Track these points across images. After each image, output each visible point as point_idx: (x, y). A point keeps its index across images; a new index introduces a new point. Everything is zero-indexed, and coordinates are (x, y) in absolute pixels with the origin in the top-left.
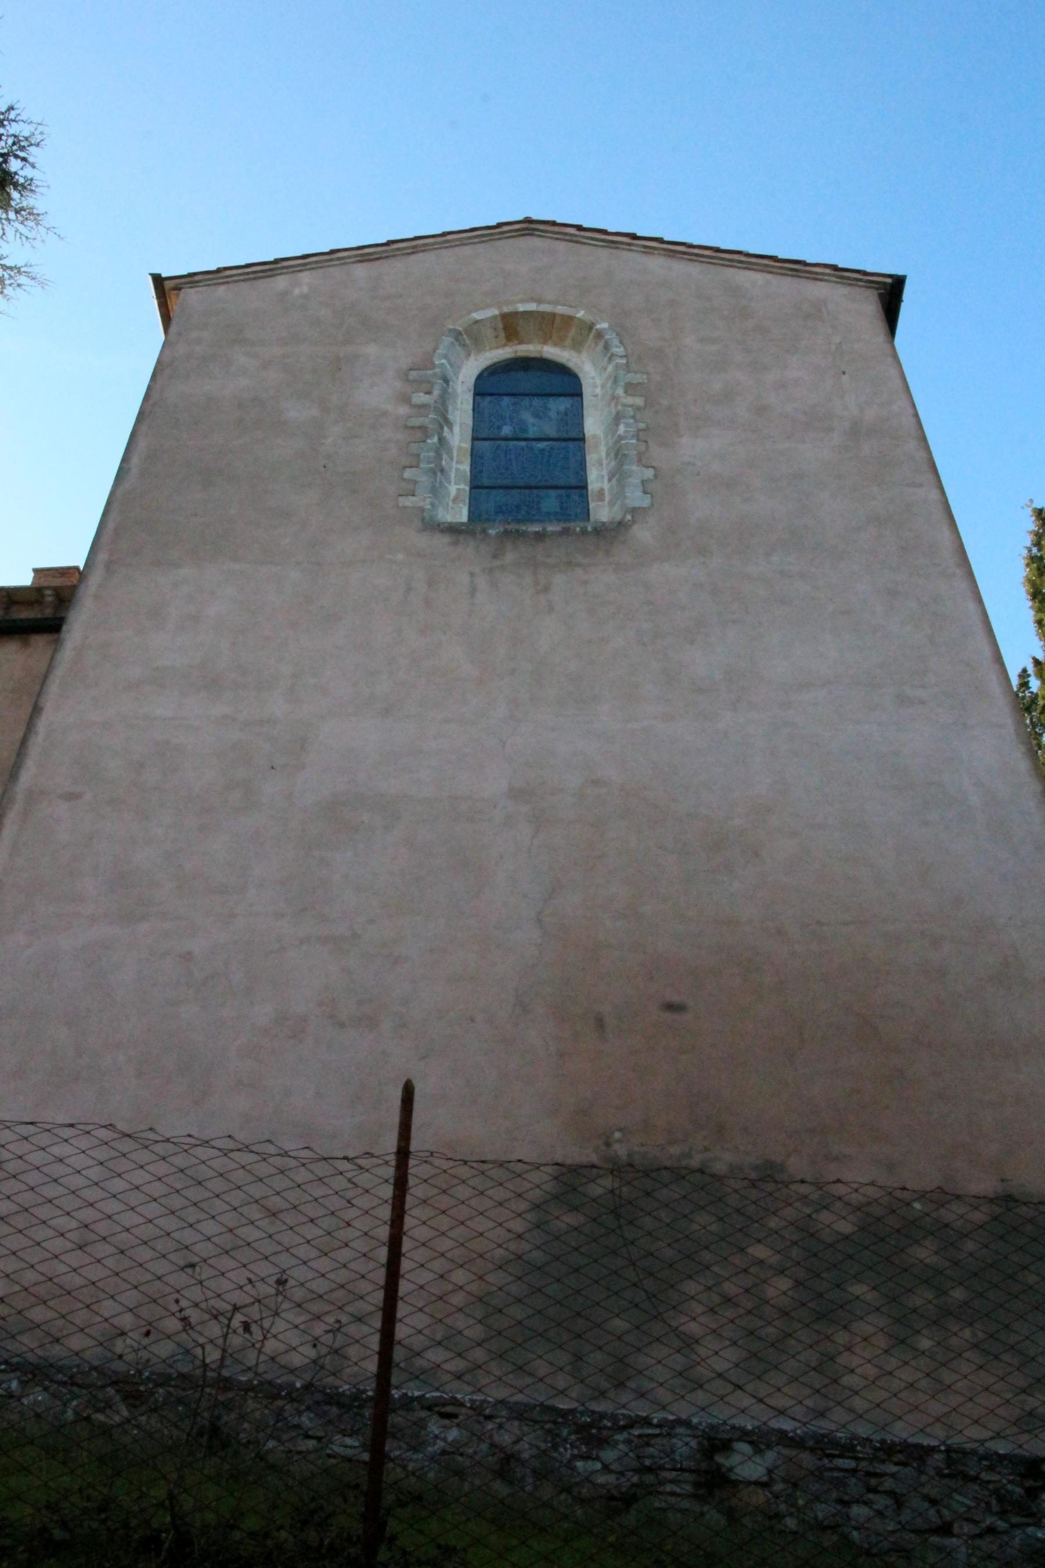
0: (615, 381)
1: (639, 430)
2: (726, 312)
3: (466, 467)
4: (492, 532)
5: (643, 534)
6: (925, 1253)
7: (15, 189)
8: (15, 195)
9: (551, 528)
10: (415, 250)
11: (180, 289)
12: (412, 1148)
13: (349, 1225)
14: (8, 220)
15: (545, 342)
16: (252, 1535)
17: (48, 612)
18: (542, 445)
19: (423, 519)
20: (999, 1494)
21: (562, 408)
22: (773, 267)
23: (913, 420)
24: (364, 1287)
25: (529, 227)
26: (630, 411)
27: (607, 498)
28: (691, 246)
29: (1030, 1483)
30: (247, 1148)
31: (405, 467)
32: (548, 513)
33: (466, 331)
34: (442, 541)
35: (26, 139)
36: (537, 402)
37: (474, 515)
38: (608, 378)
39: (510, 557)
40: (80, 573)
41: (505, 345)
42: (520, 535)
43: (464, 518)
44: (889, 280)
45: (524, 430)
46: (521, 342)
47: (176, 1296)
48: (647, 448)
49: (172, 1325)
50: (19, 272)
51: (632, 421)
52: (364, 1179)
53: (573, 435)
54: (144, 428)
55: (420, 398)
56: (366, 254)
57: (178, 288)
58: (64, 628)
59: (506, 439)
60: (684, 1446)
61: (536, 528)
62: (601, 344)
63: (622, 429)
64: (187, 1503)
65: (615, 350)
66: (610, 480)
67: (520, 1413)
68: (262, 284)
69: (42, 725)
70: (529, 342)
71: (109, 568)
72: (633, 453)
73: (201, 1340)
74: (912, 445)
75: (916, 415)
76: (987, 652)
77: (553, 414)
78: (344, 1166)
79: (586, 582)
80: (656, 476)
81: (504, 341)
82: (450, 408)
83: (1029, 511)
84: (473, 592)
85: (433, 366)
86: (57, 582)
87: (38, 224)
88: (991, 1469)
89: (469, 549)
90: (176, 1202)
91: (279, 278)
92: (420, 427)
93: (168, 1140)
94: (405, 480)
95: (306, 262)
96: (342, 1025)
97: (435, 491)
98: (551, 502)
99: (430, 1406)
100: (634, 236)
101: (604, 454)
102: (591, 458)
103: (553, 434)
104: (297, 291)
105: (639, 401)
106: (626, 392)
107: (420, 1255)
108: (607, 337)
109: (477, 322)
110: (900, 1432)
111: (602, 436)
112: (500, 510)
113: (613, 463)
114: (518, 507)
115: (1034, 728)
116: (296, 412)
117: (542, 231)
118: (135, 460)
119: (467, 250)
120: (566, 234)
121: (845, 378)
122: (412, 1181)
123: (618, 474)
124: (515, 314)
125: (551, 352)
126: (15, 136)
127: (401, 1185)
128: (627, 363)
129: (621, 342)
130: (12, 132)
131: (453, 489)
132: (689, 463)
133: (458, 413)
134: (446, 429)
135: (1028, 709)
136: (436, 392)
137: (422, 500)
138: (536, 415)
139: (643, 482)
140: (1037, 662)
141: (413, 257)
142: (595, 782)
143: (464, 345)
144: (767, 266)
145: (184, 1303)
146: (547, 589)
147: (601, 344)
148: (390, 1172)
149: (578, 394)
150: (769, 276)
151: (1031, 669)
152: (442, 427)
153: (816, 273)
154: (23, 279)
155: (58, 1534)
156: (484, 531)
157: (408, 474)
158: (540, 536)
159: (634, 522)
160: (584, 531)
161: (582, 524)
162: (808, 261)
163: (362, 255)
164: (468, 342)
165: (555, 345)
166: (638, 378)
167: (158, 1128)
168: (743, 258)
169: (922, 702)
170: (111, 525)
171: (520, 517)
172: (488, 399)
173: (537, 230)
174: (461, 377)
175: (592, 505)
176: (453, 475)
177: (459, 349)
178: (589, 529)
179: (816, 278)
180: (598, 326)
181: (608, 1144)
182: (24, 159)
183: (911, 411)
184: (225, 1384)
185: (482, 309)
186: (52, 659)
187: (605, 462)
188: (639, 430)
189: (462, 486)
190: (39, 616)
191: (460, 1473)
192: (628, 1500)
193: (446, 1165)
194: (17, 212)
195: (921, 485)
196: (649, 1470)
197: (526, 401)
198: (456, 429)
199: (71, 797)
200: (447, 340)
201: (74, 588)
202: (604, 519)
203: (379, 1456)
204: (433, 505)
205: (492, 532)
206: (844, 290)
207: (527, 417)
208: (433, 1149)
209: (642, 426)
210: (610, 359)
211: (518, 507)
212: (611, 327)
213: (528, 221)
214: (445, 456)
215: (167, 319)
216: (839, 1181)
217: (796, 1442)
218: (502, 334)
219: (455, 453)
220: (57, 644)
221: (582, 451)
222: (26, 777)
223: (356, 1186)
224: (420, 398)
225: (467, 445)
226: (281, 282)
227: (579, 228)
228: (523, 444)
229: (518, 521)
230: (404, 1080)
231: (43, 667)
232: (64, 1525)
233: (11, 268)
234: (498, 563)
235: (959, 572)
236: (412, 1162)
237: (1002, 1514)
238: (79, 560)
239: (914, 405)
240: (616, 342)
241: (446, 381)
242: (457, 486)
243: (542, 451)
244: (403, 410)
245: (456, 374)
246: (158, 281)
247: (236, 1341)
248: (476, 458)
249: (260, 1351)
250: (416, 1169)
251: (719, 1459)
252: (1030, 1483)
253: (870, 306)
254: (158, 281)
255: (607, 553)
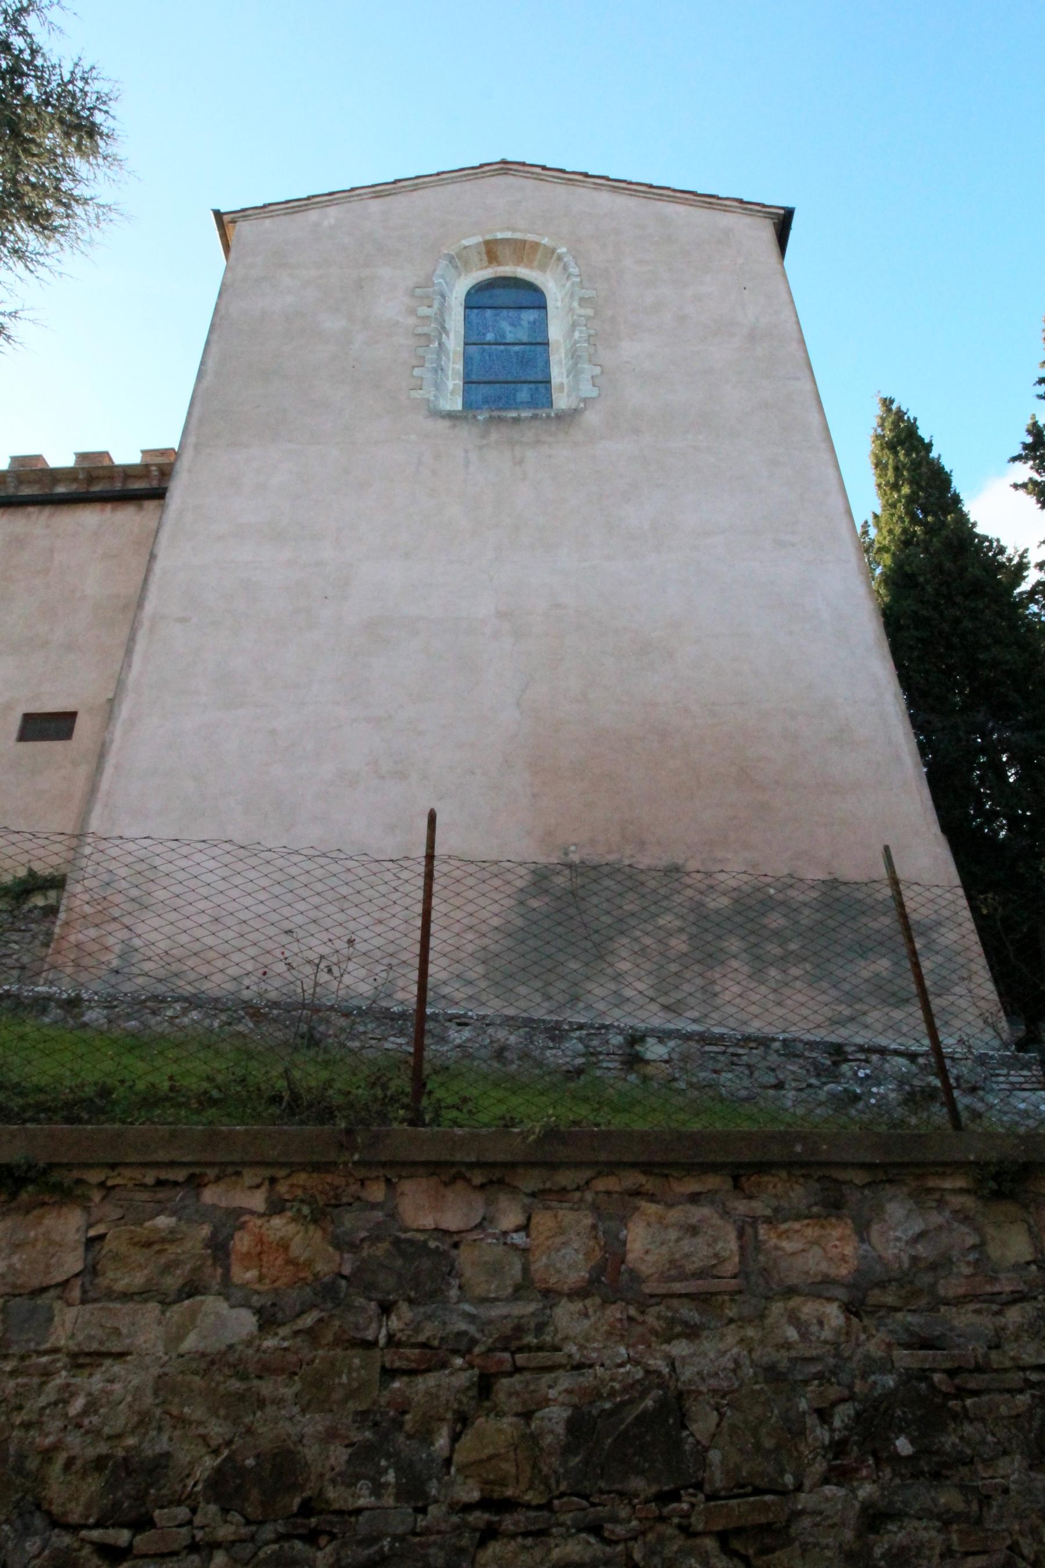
0: (572, 296)
1: (590, 336)
2: (657, 239)
3: (460, 366)
4: (480, 418)
5: (592, 418)
6: (776, 921)
7: (102, 139)
8: (101, 143)
9: (525, 414)
10: (416, 188)
11: (235, 222)
12: (436, 854)
13: (395, 903)
14: (98, 165)
15: (518, 265)
16: (340, 1091)
17: (155, 484)
18: (517, 348)
19: (429, 408)
20: (815, 1063)
21: (532, 318)
22: (695, 201)
23: (795, 326)
24: (405, 942)
25: (506, 167)
26: (583, 320)
27: (566, 391)
28: (630, 183)
29: (834, 1058)
30: (324, 855)
31: (413, 367)
32: (522, 403)
33: (457, 254)
34: (444, 425)
35: (107, 95)
36: (513, 313)
37: (467, 404)
38: (566, 294)
39: (494, 436)
40: (176, 453)
41: (486, 267)
42: (500, 419)
43: (459, 407)
44: (782, 212)
45: (504, 337)
46: (500, 264)
47: (282, 949)
48: (596, 350)
49: (281, 967)
50: (110, 209)
51: (584, 328)
52: (405, 875)
53: (539, 340)
54: (215, 337)
55: (424, 311)
56: (379, 191)
57: (233, 222)
58: (168, 495)
59: (489, 344)
60: (617, 1040)
61: (513, 414)
62: (561, 265)
63: (577, 335)
64: (297, 1074)
65: (571, 270)
66: (568, 376)
67: (510, 1022)
68: (298, 217)
69: (158, 567)
70: (507, 264)
71: (197, 447)
72: (585, 355)
73: (301, 976)
74: (794, 346)
75: (798, 323)
76: (842, 509)
77: (525, 323)
78: (390, 865)
79: (550, 456)
80: (602, 373)
81: (486, 264)
82: (447, 319)
83: (877, 400)
84: (467, 464)
85: (434, 284)
86: (160, 460)
87: (121, 169)
88: (812, 1050)
89: (465, 432)
90: (277, 890)
91: (312, 212)
92: (425, 335)
93: (270, 850)
94: (413, 376)
95: (332, 198)
96: (383, 778)
97: (438, 386)
98: (524, 394)
99: (451, 1018)
100: (586, 175)
101: (563, 355)
102: (554, 359)
103: (525, 339)
104: (326, 223)
105: (590, 312)
106: (580, 305)
107: (443, 922)
108: (565, 259)
109: (465, 248)
110: (754, 1027)
111: (562, 341)
112: (486, 401)
113: (570, 362)
114: (500, 398)
115: (870, 564)
116: (332, 323)
117: (516, 170)
118: (210, 364)
119: (456, 188)
120: (533, 173)
121: (746, 292)
122: (436, 874)
123: (574, 371)
124: (496, 241)
125: (523, 272)
126: (98, 93)
127: (429, 876)
128: (581, 281)
129: (576, 264)
130: (95, 89)
131: (450, 385)
132: (627, 362)
133: (453, 323)
134: (444, 336)
135: (867, 551)
136: (436, 305)
137: (428, 392)
138: (513, 325)
139: (593, 377)
140: (876, 516)
141: (415, 193)
142: (558, 606)
143: (456, 267)
144: (687, 199)
145: (287, 954)
146: (520, 462)
147: (561, 265)
148: (421, 869)
149: (542, 307)
150: (690, 208)
151: (871, 521)
152: (441, 334)
153: (726, 206)
154: (113, 215)
155: (215, 1094)
156: (475, 417)
157: (417, 372)
158: (516, 420)
159: (585, 409)
160: (548, 416)
161: (548, 410)
162: (721, 195)
163: (375, 192)
164: (459, 264)
165: (526, 266)
166: (588, 293)
167: (263, 843)
168: (672, 194)
169: (793, 545)
170: (196, 414)
171: (501, 405)
172: (475, 311)
173: (511, 170)
174: (454, 295)
175: (554, 397)
176: (450, 373)
177: (453, 270)
178: (553, 415)
179: (726, 209)
180: (559, 251)
181: (566, 854)
182: (106, 112)
183: (794, 319)
184: (316, 1010)
185: (470, 236)
186: (161, 518)
187: (564, 362)
188: (590, 336)
189: (457, 382)
190: (148, 486)
191: (470, 1056)
192: (579, 1071)
193: (459, 864)
194: (105, 158)
195: (798, 379)
196: (592, 1054)
197: (504, 312)
198: (452, 335)
199: (183, 620)
200: (444, 263)
201: (172, 465)
202: (563, 407)
203: (420, 1047)
204: (435, 396)
205: (480, 418)
206: (747, 220)
207: (505, 326)
208: (450, 853)
209: (592, 332)
210: (568, 278)
211: (500, 398)
212: (568, 251)
213: (504, 162)
214: (444, 358)
215: (227, 248)
216: (722, 871)
217: (688, 1037)
218: (485, 258)
219: (451, 355)
220: (163, 508)
221: (547, 351)
222: (149, 607)
223: (399, 878)
224: (424, 311)
225: (460, 349)
226: (313, 215)
227: (544, 168)
228: (502, 347)
229: (499, 409)
230: (428, 810)
231: (153, 525)
232: (219, 1088)
233: (103, 206)
234: (485, 442)
235: (823, 446)
236: (436, 863)
237: (818, 1076)
238: (176, 447)
239: (797, 316)
240: (573, 264)
241: (443, 296)
242: (454, 381)
243: (517, 353)
244: (411, 321)
245: (451, 291)
246: (218, 215)
247: (323, 977)
248: (467, 360)
249: (340, 982)
250: (438, 866)
251: (638, 1048)
252: (834, 1058)
253: (767, 233)
254: (218, 215)
255: (566, 433)
